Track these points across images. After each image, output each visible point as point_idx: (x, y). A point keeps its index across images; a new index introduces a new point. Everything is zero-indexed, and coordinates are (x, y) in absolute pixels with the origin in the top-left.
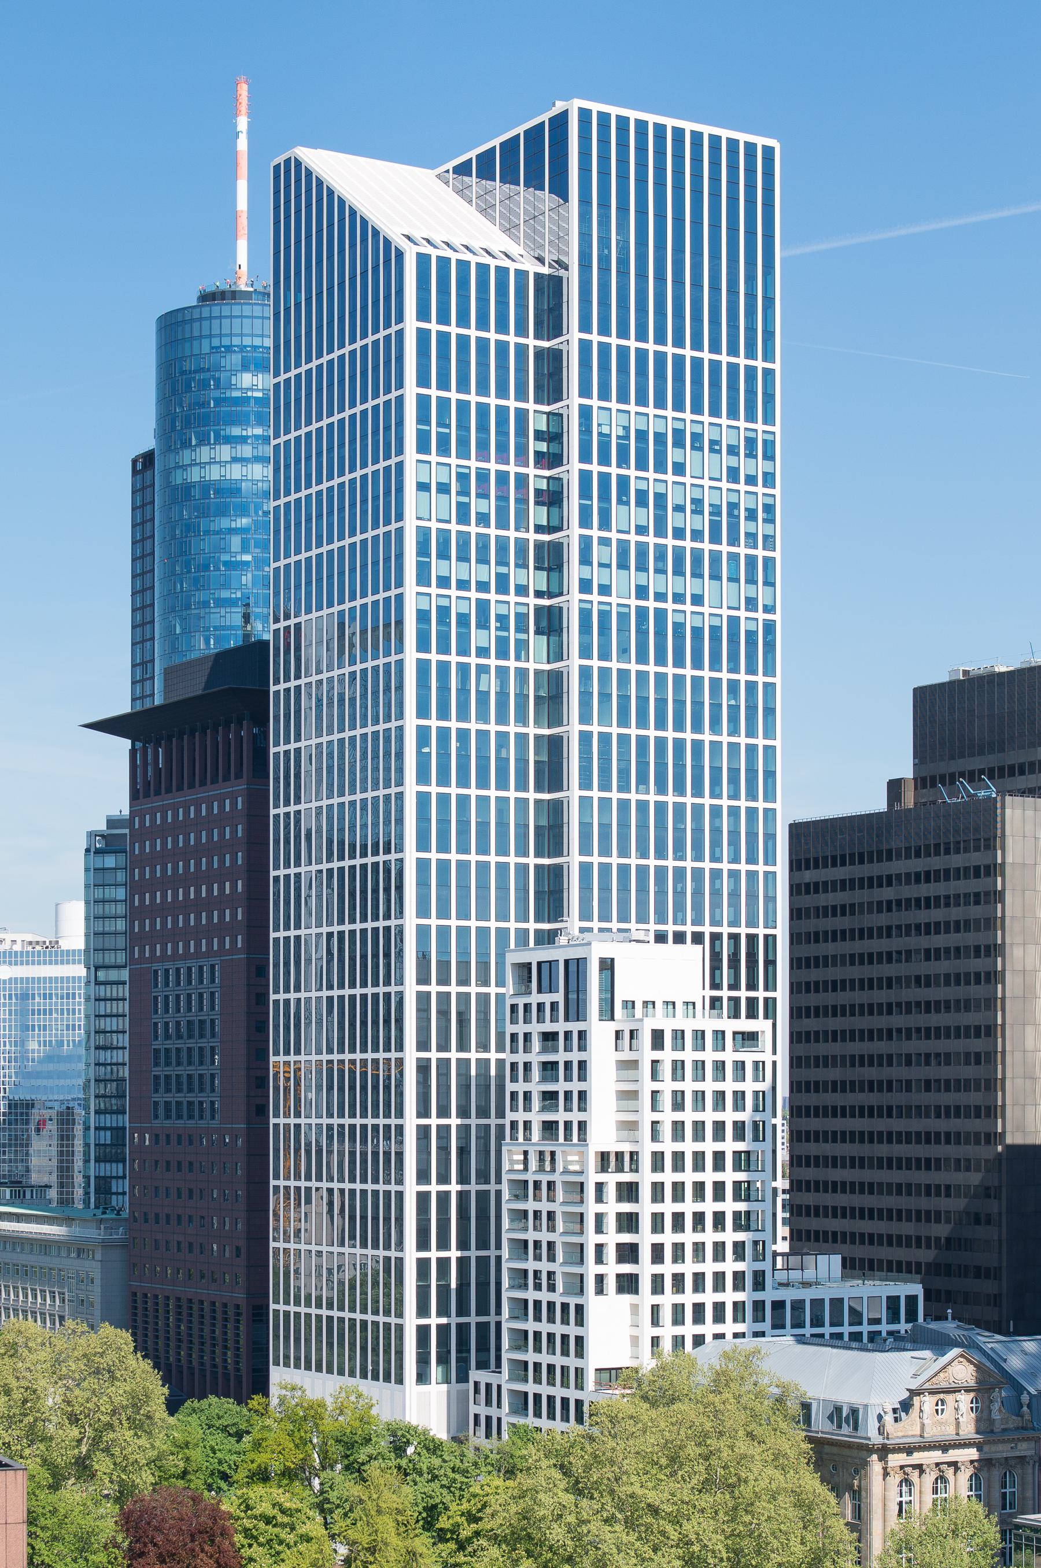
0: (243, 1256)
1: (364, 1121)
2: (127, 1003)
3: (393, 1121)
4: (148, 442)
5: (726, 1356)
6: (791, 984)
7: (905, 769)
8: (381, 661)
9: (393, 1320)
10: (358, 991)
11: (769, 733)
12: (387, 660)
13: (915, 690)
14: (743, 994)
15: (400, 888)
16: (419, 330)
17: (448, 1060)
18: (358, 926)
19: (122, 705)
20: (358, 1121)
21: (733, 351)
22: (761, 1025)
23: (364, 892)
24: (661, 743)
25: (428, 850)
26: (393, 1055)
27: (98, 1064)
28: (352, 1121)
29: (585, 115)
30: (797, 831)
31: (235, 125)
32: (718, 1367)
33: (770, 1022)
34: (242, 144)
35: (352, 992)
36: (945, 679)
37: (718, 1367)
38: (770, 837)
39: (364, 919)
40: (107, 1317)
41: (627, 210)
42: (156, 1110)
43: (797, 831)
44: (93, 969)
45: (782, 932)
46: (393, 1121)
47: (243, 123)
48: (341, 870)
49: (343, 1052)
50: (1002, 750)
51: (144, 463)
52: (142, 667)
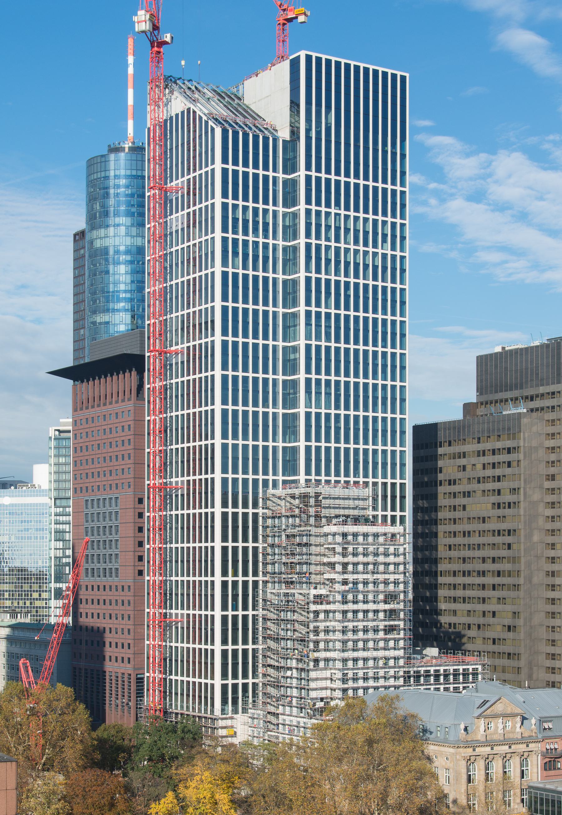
0: (132, 487)
2: (71, 517)
4: (81, 224)
7: (472, 397)
8: (203, 341)
9: (209, 681)
10: (191, 511)
11: (402, 314)
12: (206, 340)
13: (477, 357)
14: (389, 513)
15: (213, 458)
16: (223, 203)
18: (191, 511)
19: (68, 362)
20: (191, 579)
21: (385, 181)
22: (398, 529)
24: (347, 375)
25: (227, 404)
26: (209, 544)
27: (56, 549)
28: (188, 579)
29: (309, 58)
30: (417, 429)
31: (127, 60)
33: (402, 527)
34: (131, 70)
36: (498, 349)
37: (377, 705)
38: (403, 433)
39: (194, 441)
40: (60, 680)
42: (87, 505)
43: (417, 429)
44: (53, 499)
45: (409, 481)
46: (209, 579)
47: (131, 59)
48: (183, 449)
49: (183, 576)
50: (521, 388)
51: (80, 236)
52: (78, 341)
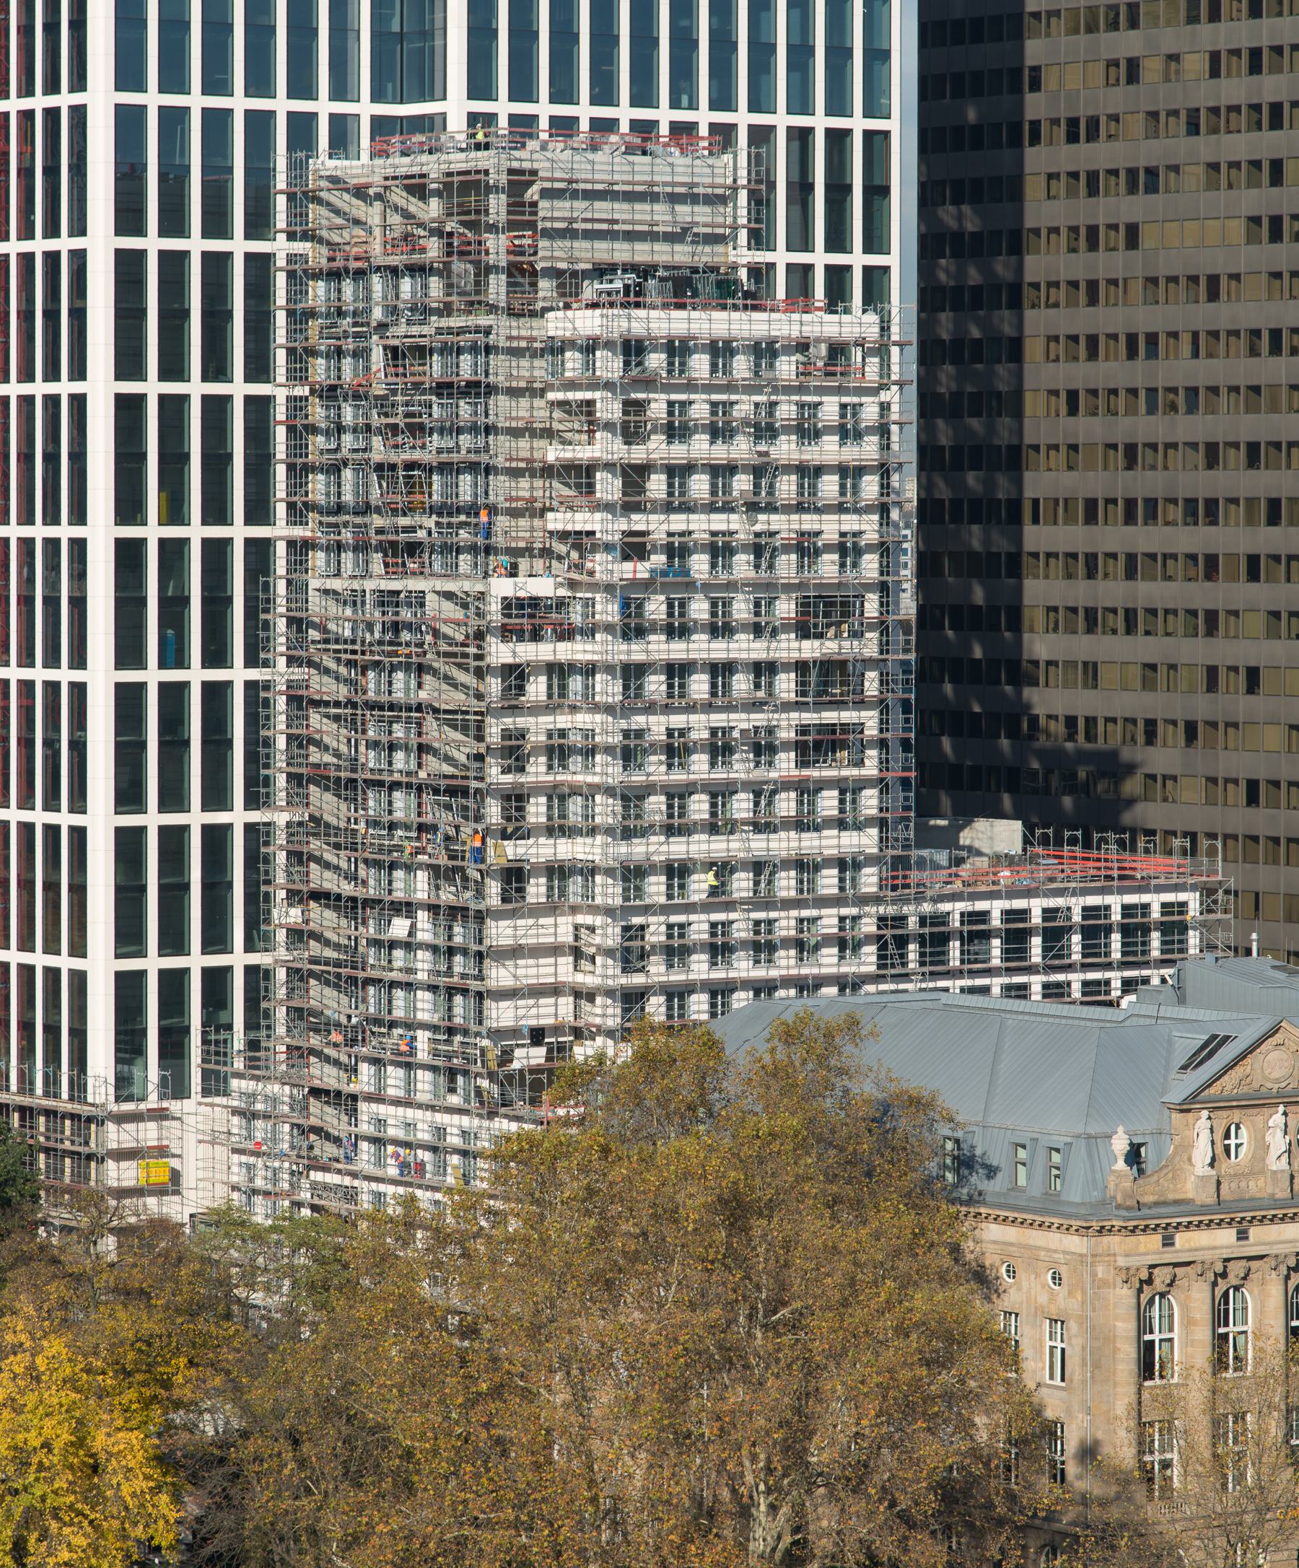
1: (26, 531)
3: (65, 532)
5: (789, 1035)
6: (923, 240)
17: (634, 103)
23: (52, 316)
28: (26, 531)
32: (767, 1059)
33: (872, 318)
35: (26, 246)
37: (767, 1059)
41: (71, 456)
